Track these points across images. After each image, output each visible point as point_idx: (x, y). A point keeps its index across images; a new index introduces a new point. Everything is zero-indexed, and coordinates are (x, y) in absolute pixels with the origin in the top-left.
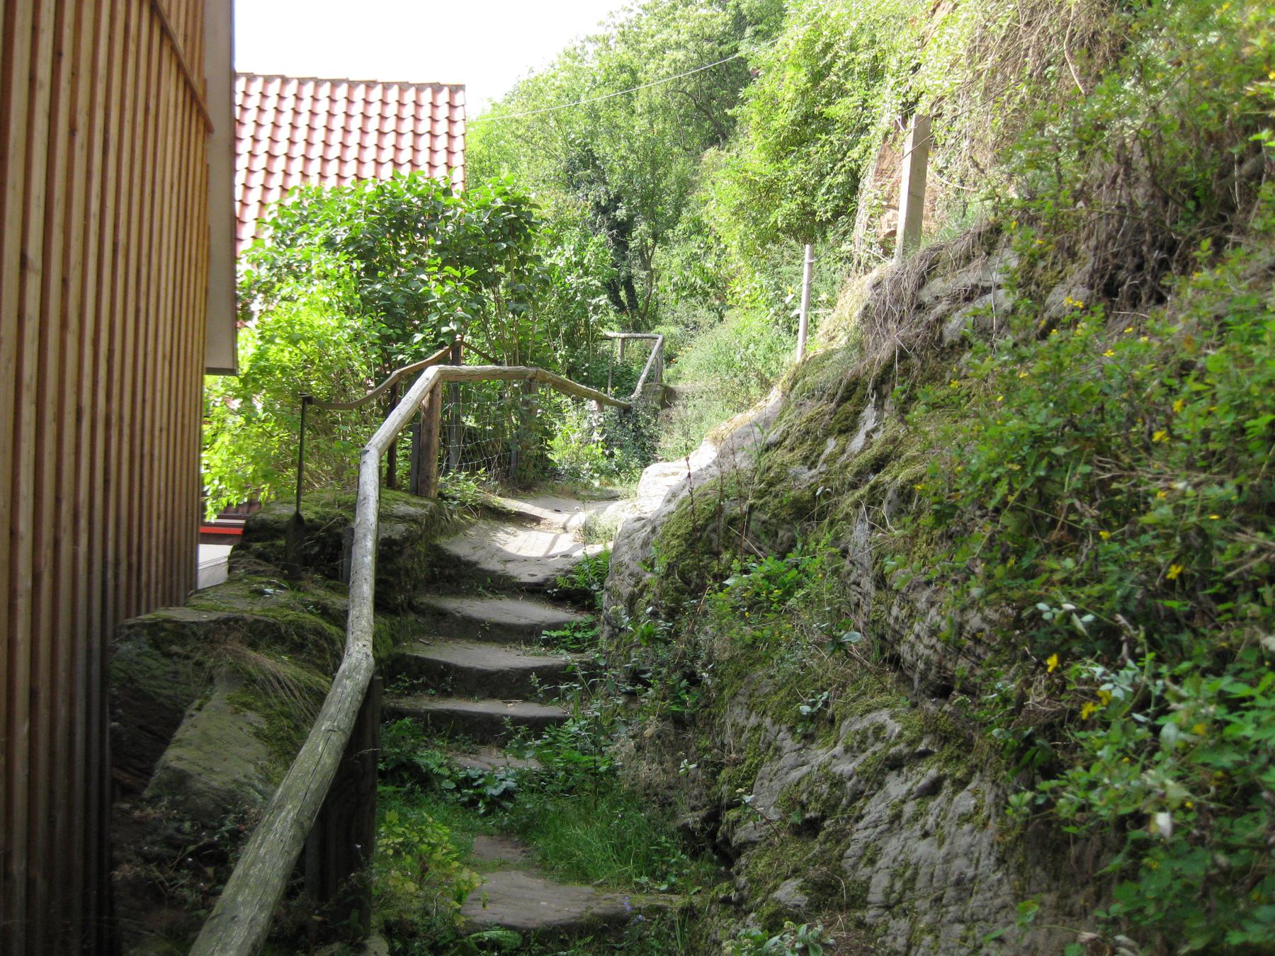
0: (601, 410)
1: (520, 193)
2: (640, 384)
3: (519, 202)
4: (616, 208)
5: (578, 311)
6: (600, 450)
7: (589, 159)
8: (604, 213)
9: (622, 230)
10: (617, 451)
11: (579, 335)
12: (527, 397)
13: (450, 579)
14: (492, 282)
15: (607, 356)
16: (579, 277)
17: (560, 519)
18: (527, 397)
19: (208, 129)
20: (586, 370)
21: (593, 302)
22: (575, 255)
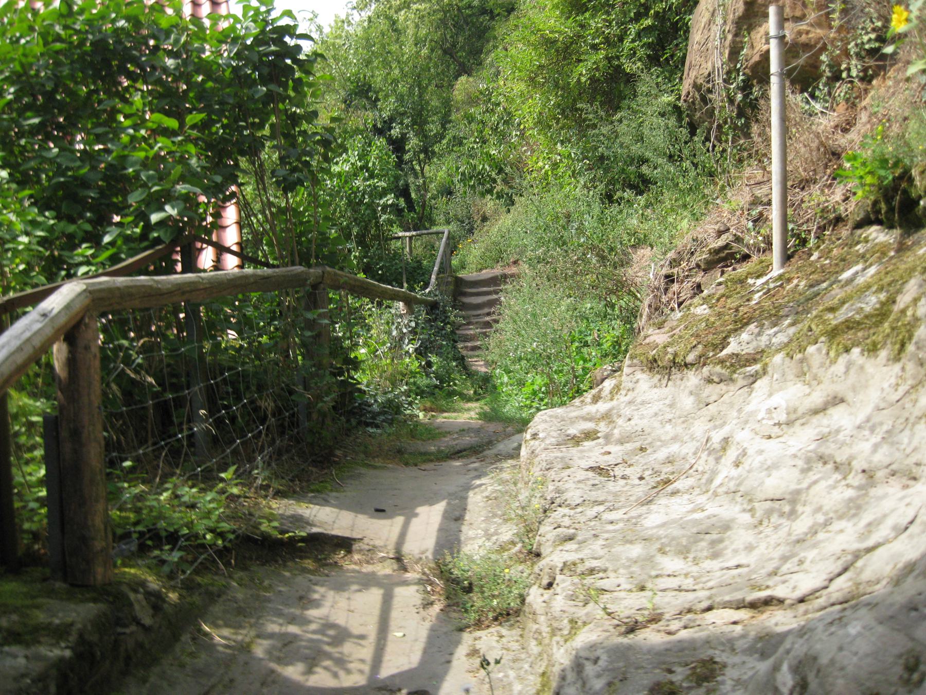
0: (411, 311)
2: (433, 277)
4: (390, 128)
5: (368, 212)
6: (417, 364)
9: (398, 145)
10: (433, 359)
11: (369, 234)
12: (310, 316)
15: (397, 255)
16: (365, 180)
17: (379, 532)
18: (310, 316)
20: (380, 269)
21: (382, 202)
22: (360, 160)
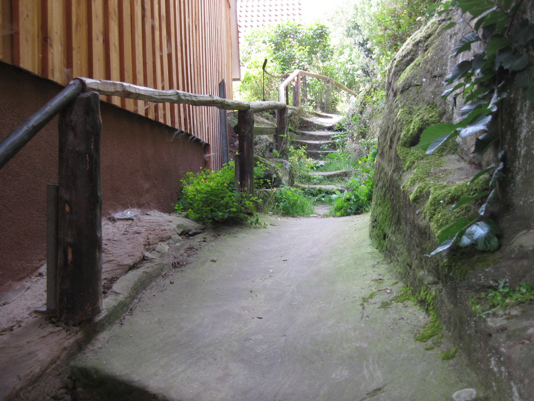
1: (322, 24)
3: (322, 27)
7: (356, 27)
8: (362, 46)
13: (306, 127)
14: (315, 53)
19: (230, 7)
